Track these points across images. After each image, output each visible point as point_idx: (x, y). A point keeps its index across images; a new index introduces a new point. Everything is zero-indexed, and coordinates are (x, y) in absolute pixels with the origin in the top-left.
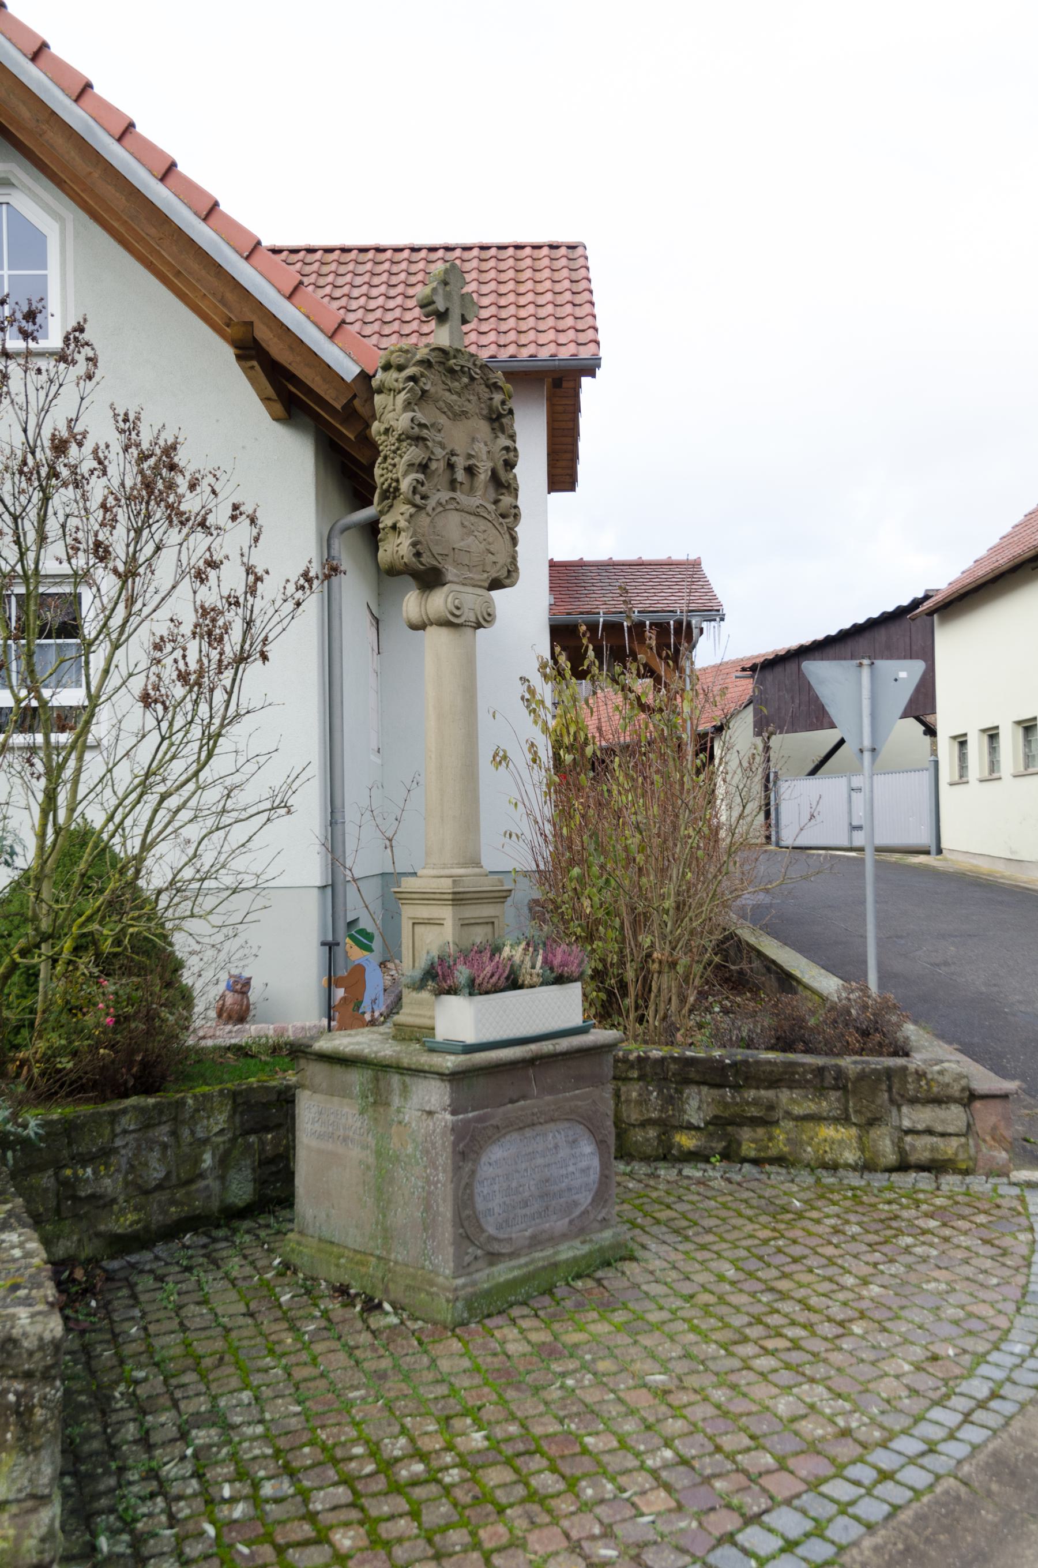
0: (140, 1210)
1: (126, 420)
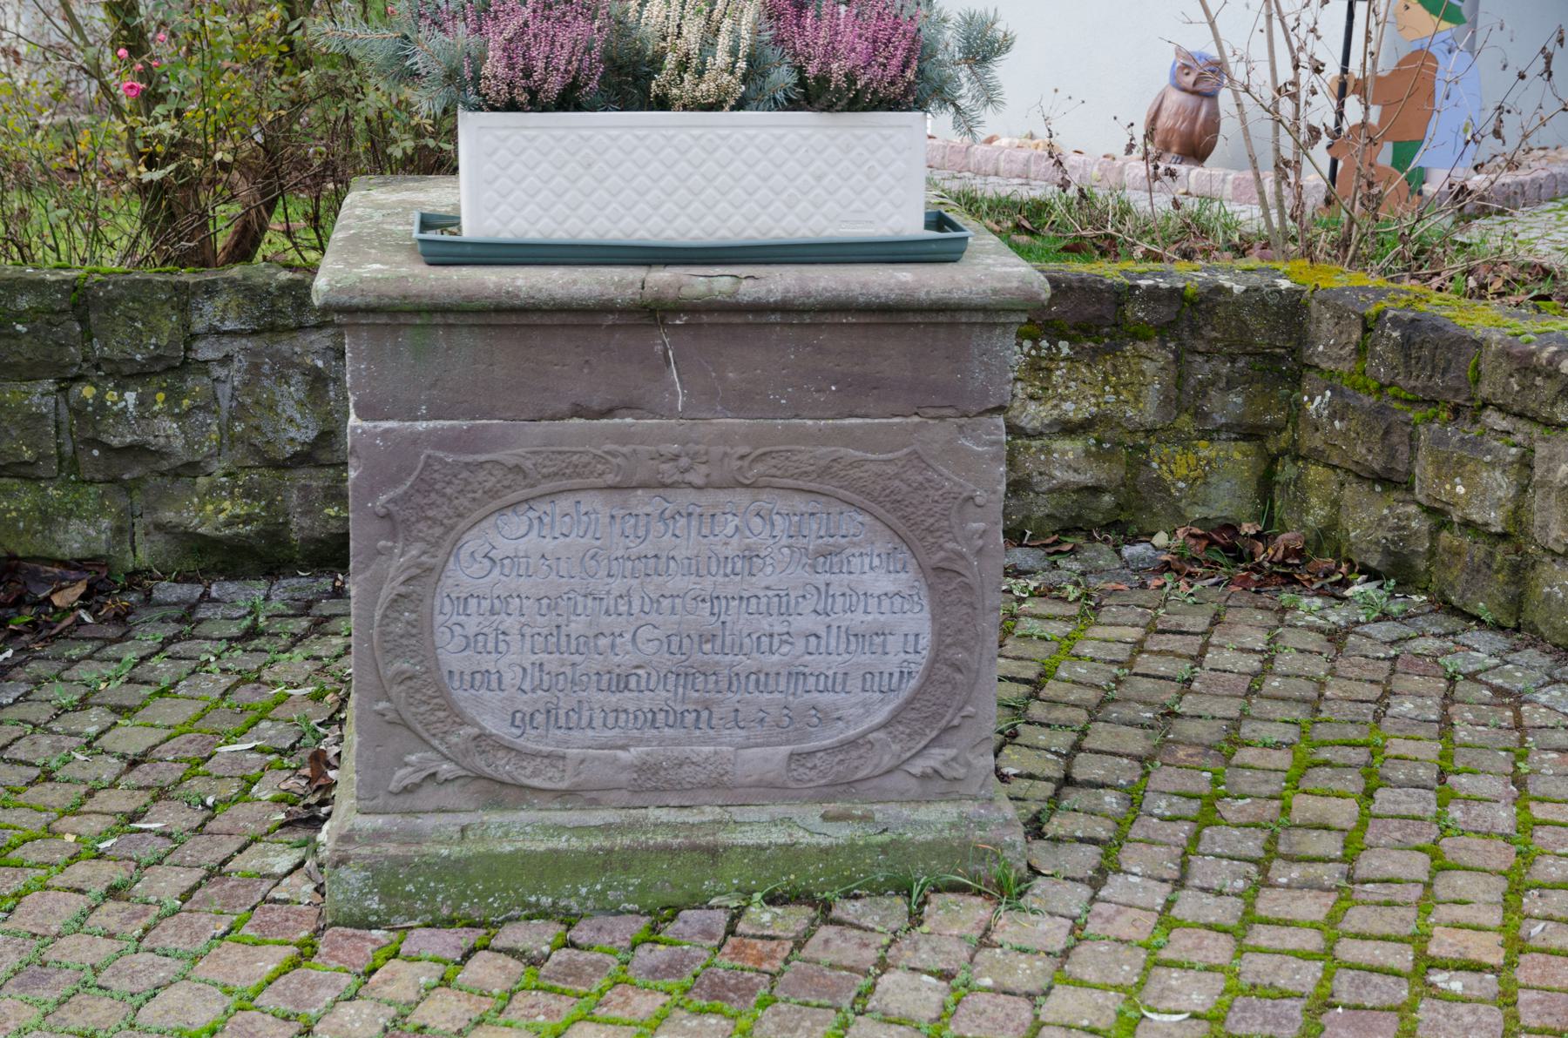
0: (256, 498)
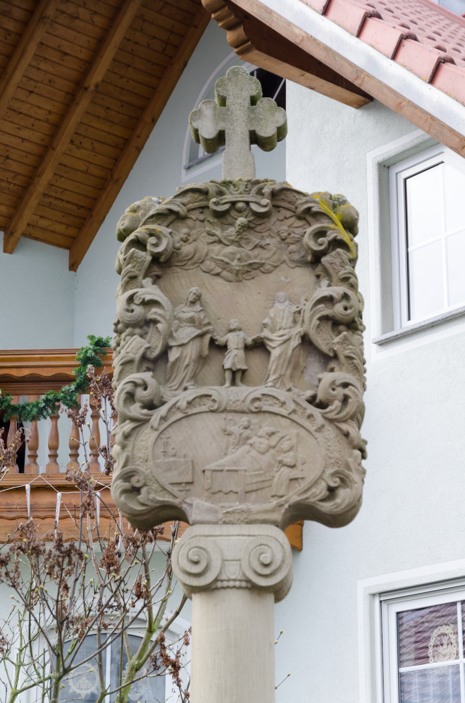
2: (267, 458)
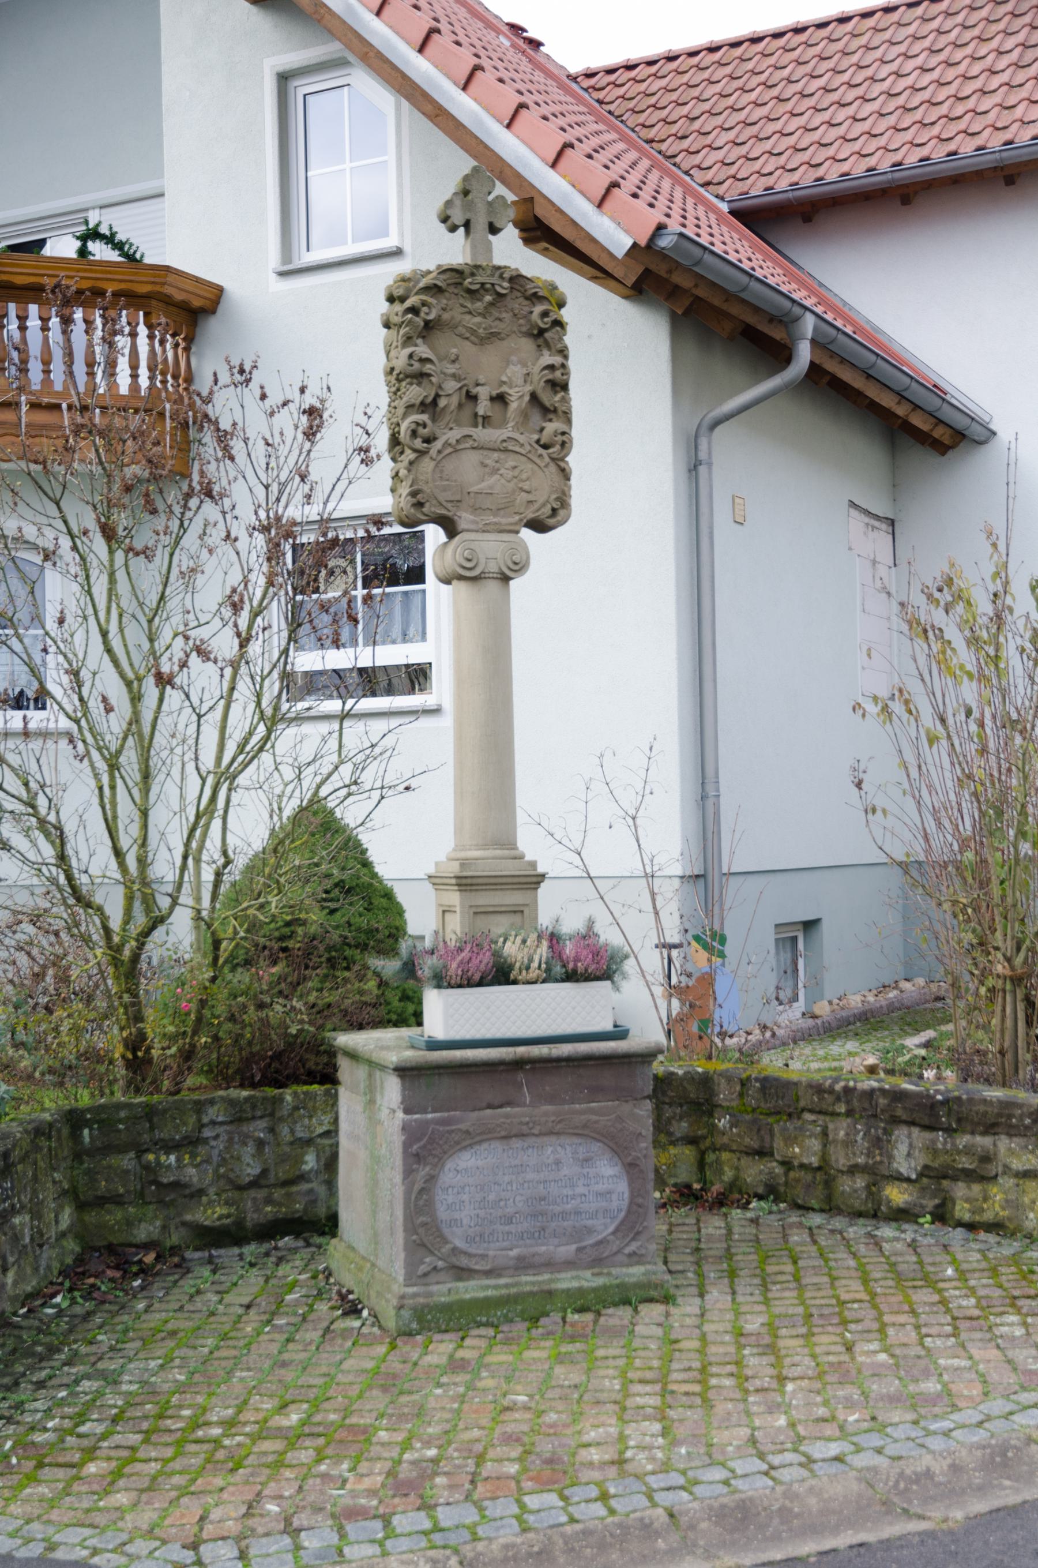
0: (232, 1205)
1: (242, 371)
2: (511, 485)
